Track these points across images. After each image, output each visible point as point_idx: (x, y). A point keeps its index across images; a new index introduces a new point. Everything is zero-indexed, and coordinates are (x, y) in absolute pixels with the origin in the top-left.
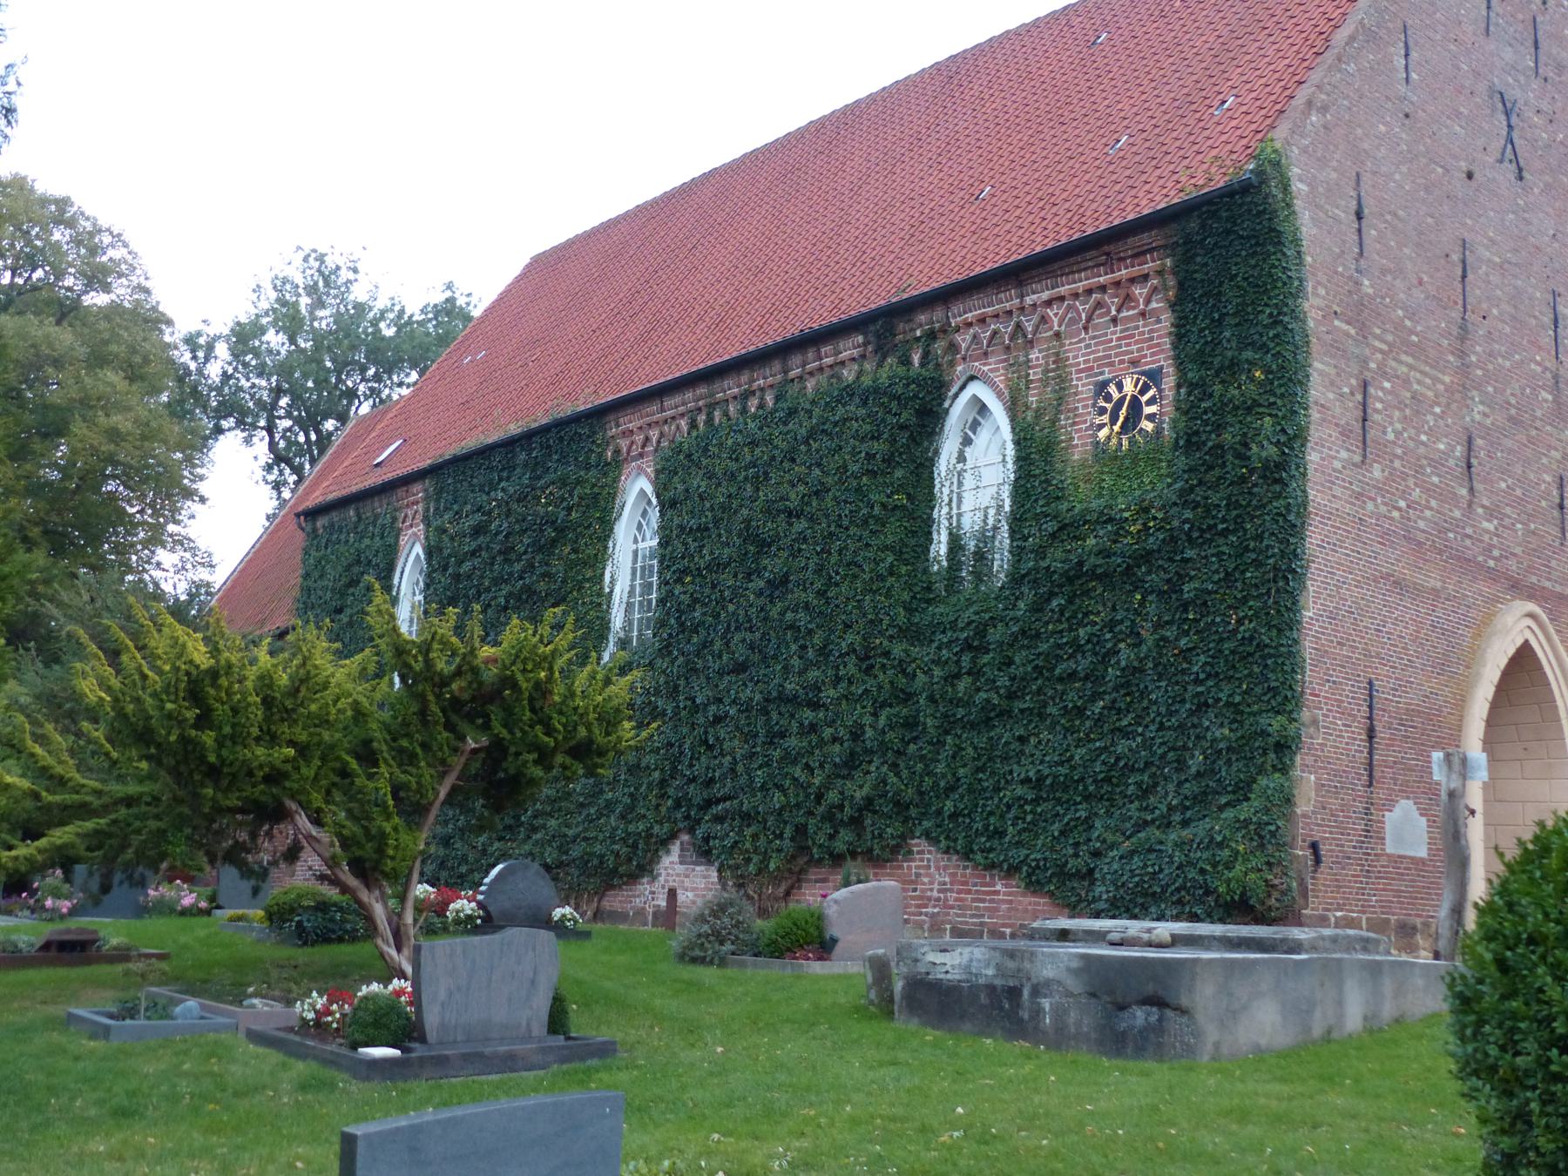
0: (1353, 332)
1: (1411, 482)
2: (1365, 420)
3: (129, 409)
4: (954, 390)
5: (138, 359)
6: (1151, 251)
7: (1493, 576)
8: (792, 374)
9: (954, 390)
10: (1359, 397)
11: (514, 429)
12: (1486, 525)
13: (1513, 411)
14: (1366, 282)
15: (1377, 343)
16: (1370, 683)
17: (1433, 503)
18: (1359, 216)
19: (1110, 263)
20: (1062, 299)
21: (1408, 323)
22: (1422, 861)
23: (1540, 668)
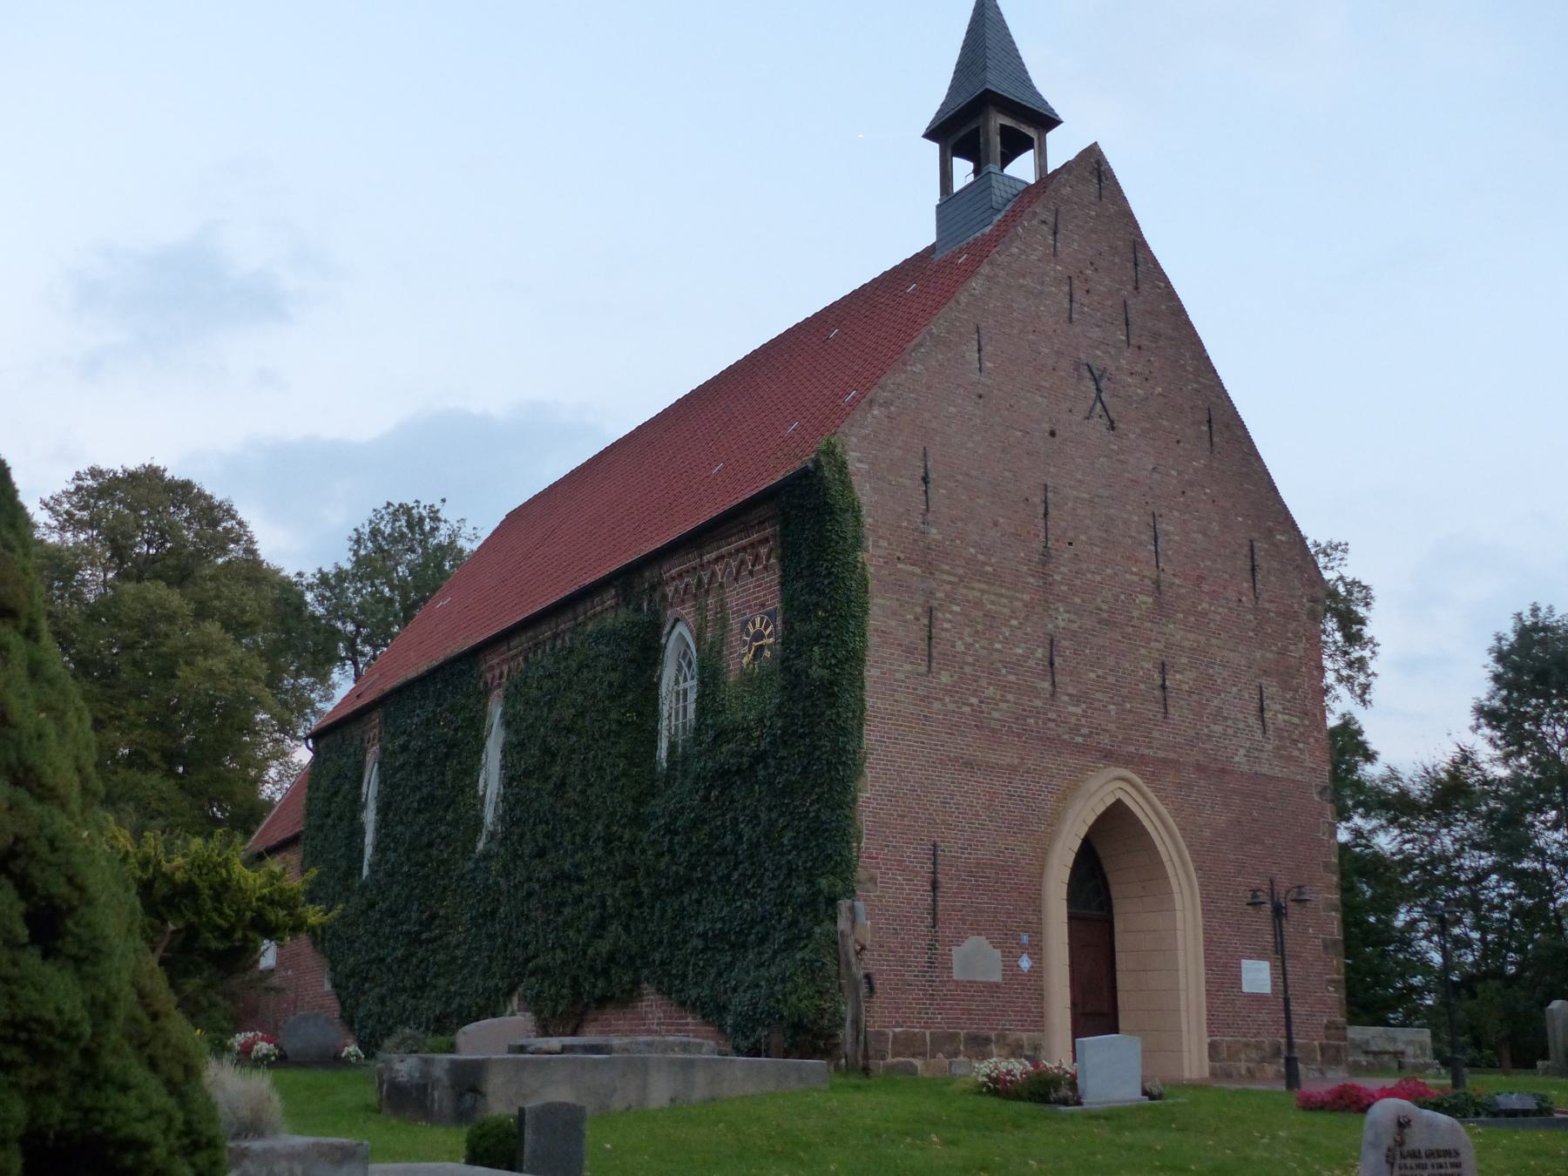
0: (918, 570)
1: (984, 683)
2: (930, 638)
3: (224, 652)
4: (667, 628)
5: (235, 611)
6: (767, 520)
7: (1082, 750)
8: (581, 619)
9: (667, 628)
10: (926, 621)
11: (423, 668)
12: (1071, 709)
13: (1105, 615)
14: (934, 531)
15: (945, 577)
16: (935, 845)
17: (1010, 697)
18: (925, 480)
19: (747, 530)
20: (722, 557)
21: (981, 557)
22: (997, 985)
23: (1138, 821)
